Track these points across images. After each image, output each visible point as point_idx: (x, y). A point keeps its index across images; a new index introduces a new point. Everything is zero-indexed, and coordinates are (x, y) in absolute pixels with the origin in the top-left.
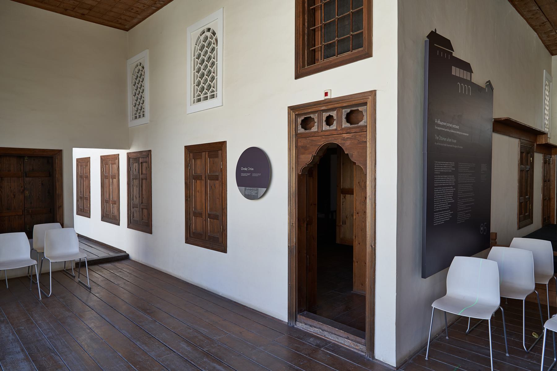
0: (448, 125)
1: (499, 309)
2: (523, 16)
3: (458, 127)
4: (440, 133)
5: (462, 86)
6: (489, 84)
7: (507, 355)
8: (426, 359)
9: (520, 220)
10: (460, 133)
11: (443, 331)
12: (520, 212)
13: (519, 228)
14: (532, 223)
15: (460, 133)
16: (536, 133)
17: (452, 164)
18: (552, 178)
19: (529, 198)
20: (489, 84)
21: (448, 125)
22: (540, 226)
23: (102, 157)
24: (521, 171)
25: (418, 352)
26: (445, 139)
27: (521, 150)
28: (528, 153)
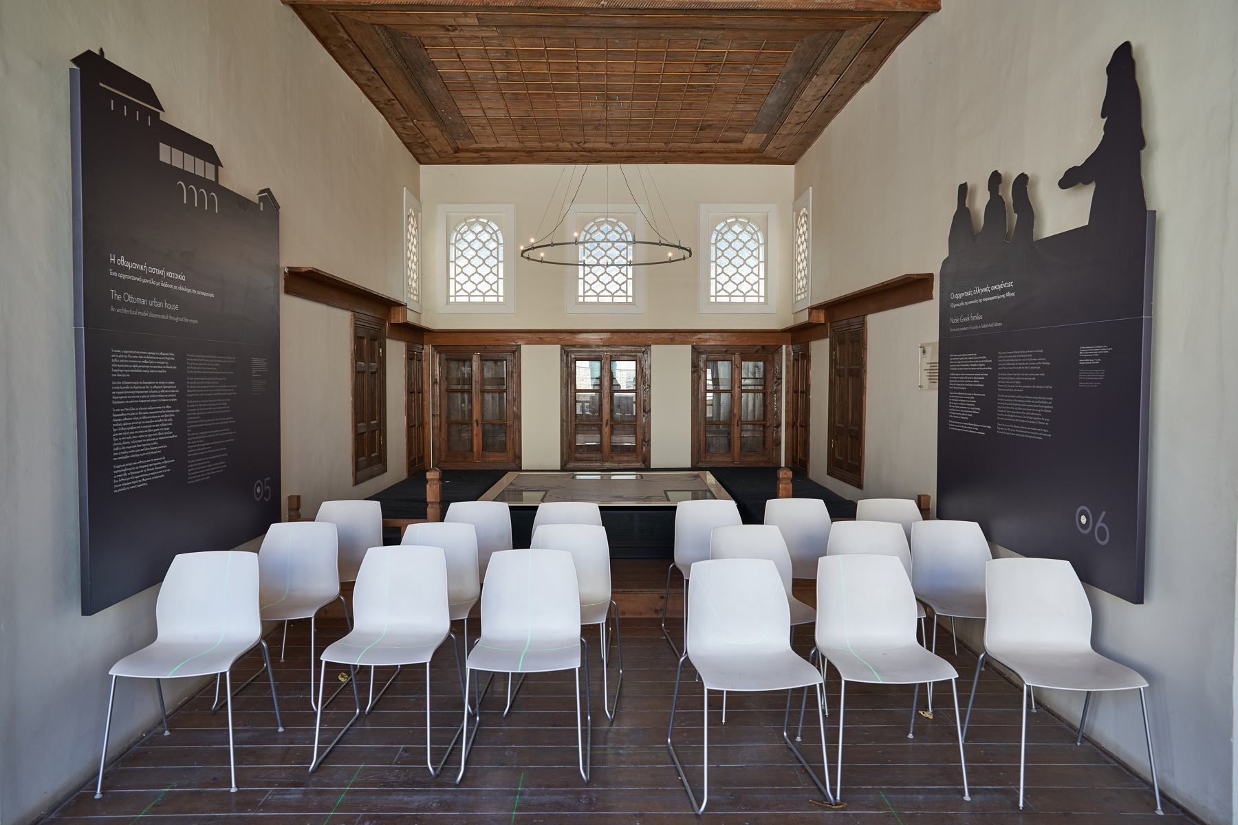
0: (152, 270)
1: (260, 643)
2: (351, 77)
3: (182, 277)
4: (124, 286)
5: (190, 192)
6: (267, 196)
7: (281, 729)
8: (98, 796)
9: (357, 467)
10: (189, 291)
11: (161, 723)
12: (358, 452)
13: (357, 482)
14: (386, 471)
15: (189, 291)
16: (388, 305)
17: (171, 356)
18: (426, 387)
19: (378, 425)
20: (267, 196)
21: (152, 270)
22: (405, 476)
23: (932, 275)
24: (358, 373)
25: (82, 785)
26: (144, 302)
27: (355, 333)
28: (373, 339)
